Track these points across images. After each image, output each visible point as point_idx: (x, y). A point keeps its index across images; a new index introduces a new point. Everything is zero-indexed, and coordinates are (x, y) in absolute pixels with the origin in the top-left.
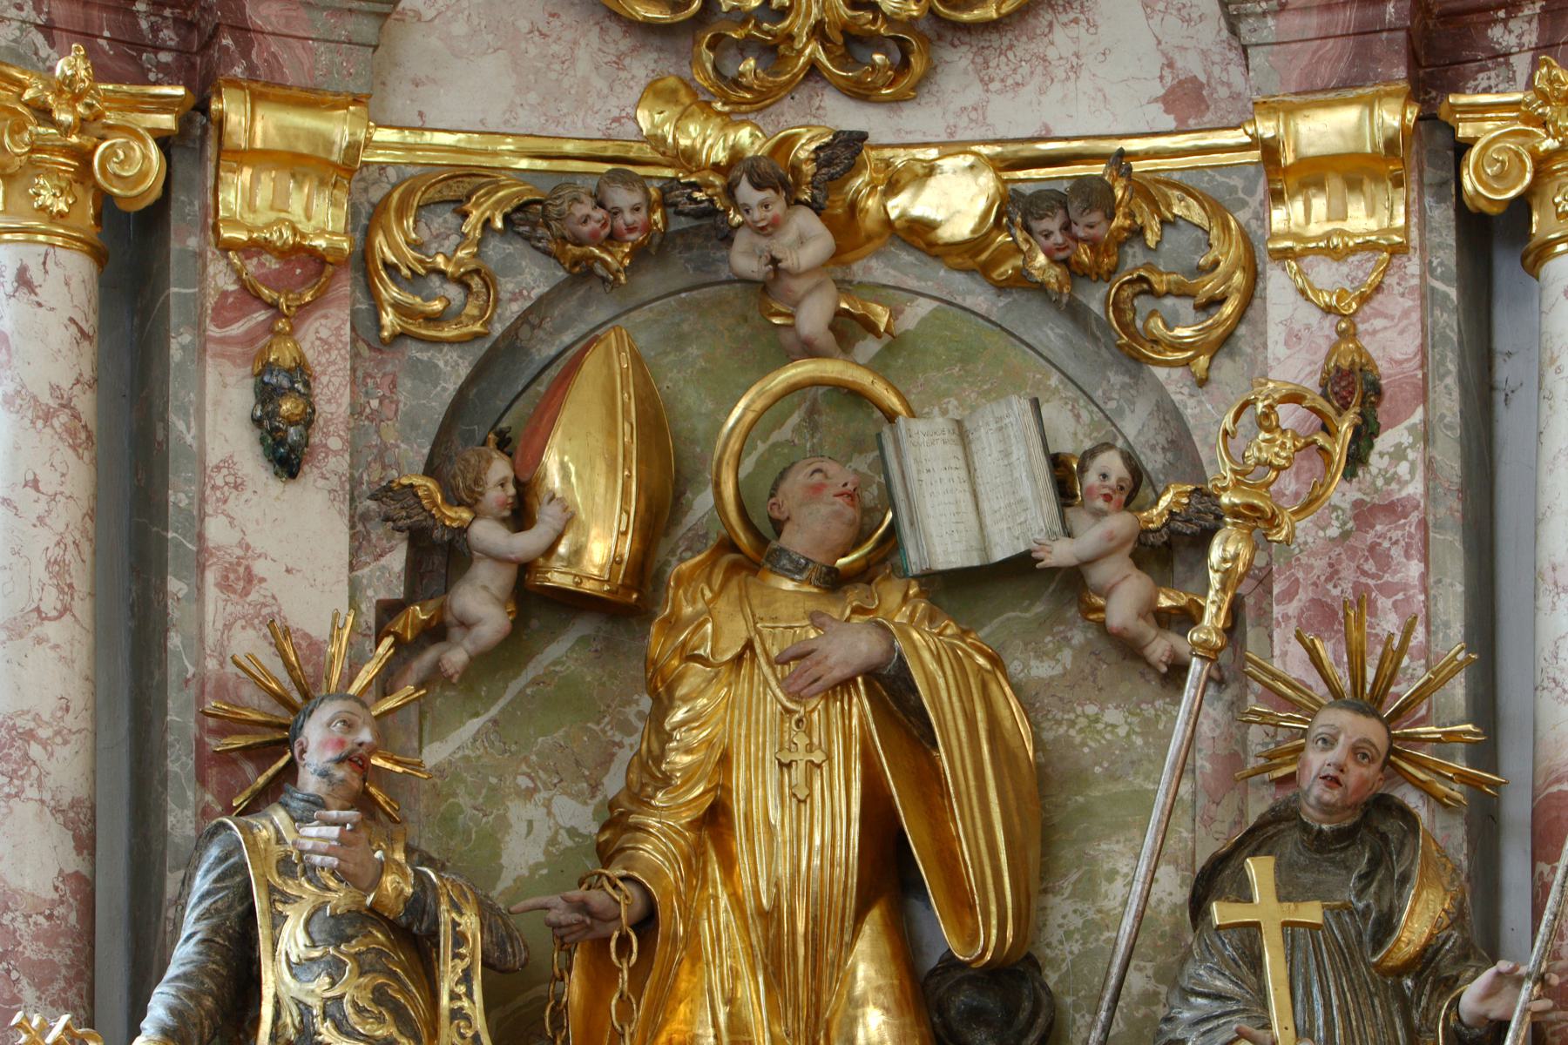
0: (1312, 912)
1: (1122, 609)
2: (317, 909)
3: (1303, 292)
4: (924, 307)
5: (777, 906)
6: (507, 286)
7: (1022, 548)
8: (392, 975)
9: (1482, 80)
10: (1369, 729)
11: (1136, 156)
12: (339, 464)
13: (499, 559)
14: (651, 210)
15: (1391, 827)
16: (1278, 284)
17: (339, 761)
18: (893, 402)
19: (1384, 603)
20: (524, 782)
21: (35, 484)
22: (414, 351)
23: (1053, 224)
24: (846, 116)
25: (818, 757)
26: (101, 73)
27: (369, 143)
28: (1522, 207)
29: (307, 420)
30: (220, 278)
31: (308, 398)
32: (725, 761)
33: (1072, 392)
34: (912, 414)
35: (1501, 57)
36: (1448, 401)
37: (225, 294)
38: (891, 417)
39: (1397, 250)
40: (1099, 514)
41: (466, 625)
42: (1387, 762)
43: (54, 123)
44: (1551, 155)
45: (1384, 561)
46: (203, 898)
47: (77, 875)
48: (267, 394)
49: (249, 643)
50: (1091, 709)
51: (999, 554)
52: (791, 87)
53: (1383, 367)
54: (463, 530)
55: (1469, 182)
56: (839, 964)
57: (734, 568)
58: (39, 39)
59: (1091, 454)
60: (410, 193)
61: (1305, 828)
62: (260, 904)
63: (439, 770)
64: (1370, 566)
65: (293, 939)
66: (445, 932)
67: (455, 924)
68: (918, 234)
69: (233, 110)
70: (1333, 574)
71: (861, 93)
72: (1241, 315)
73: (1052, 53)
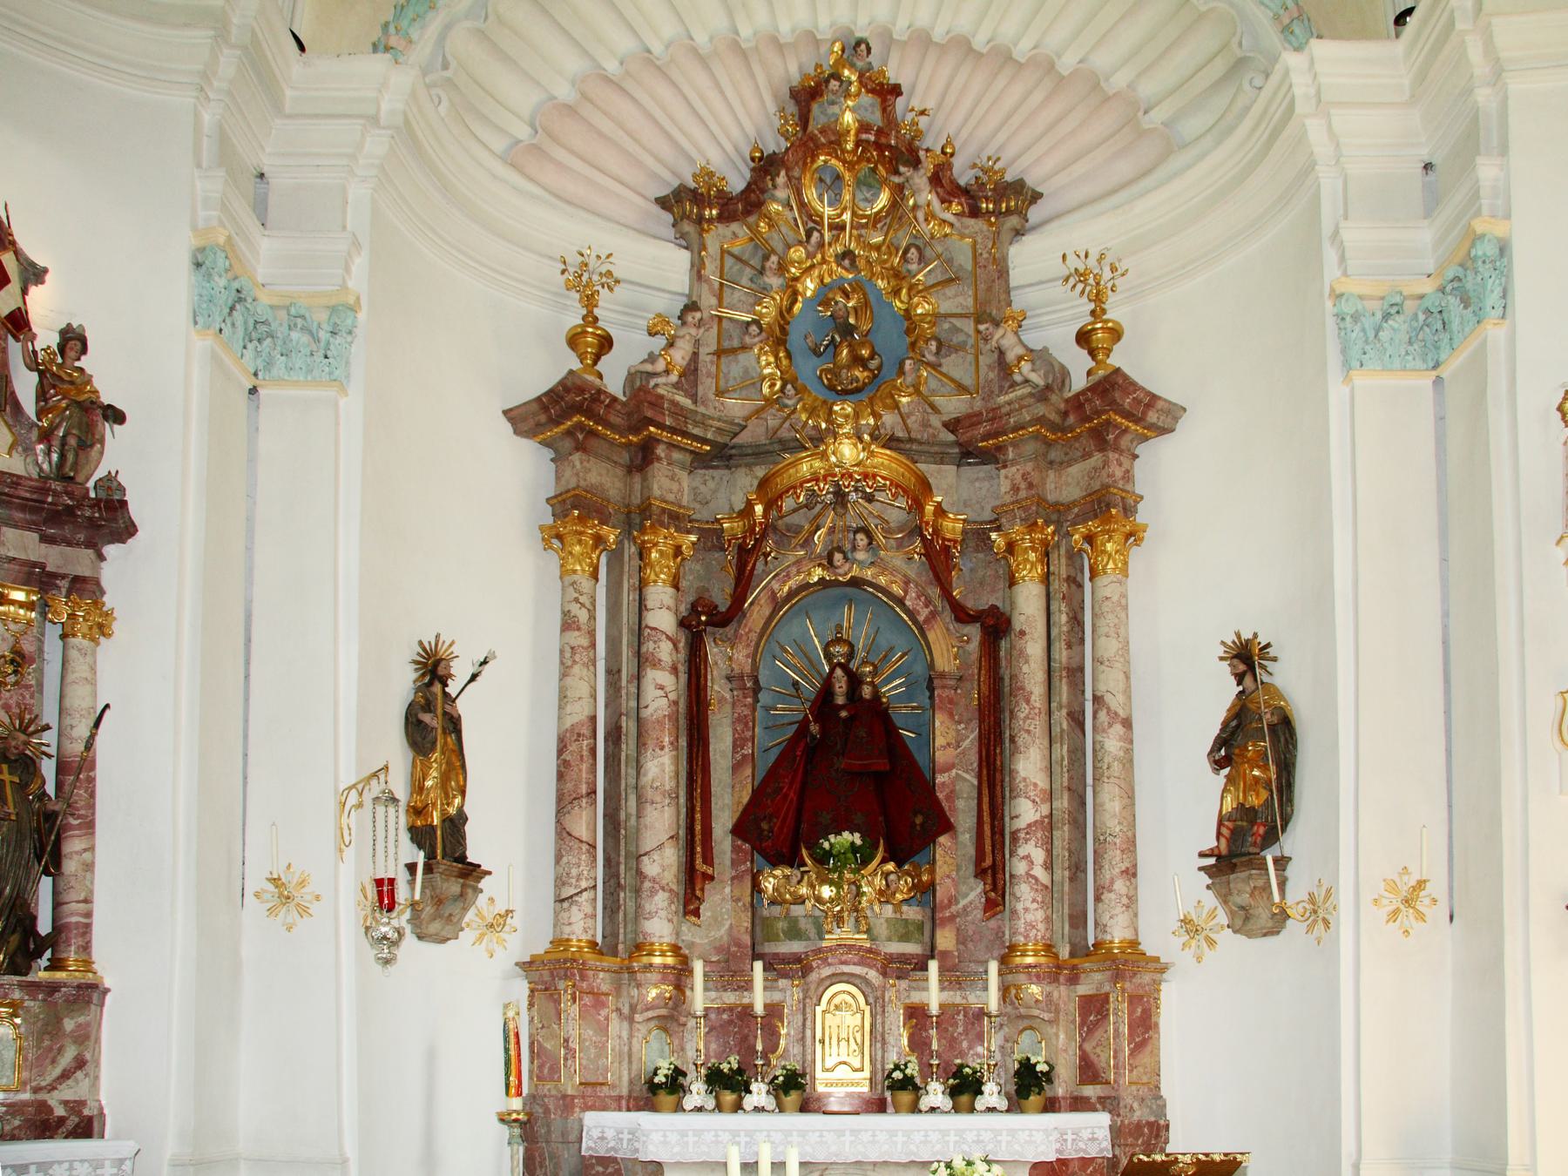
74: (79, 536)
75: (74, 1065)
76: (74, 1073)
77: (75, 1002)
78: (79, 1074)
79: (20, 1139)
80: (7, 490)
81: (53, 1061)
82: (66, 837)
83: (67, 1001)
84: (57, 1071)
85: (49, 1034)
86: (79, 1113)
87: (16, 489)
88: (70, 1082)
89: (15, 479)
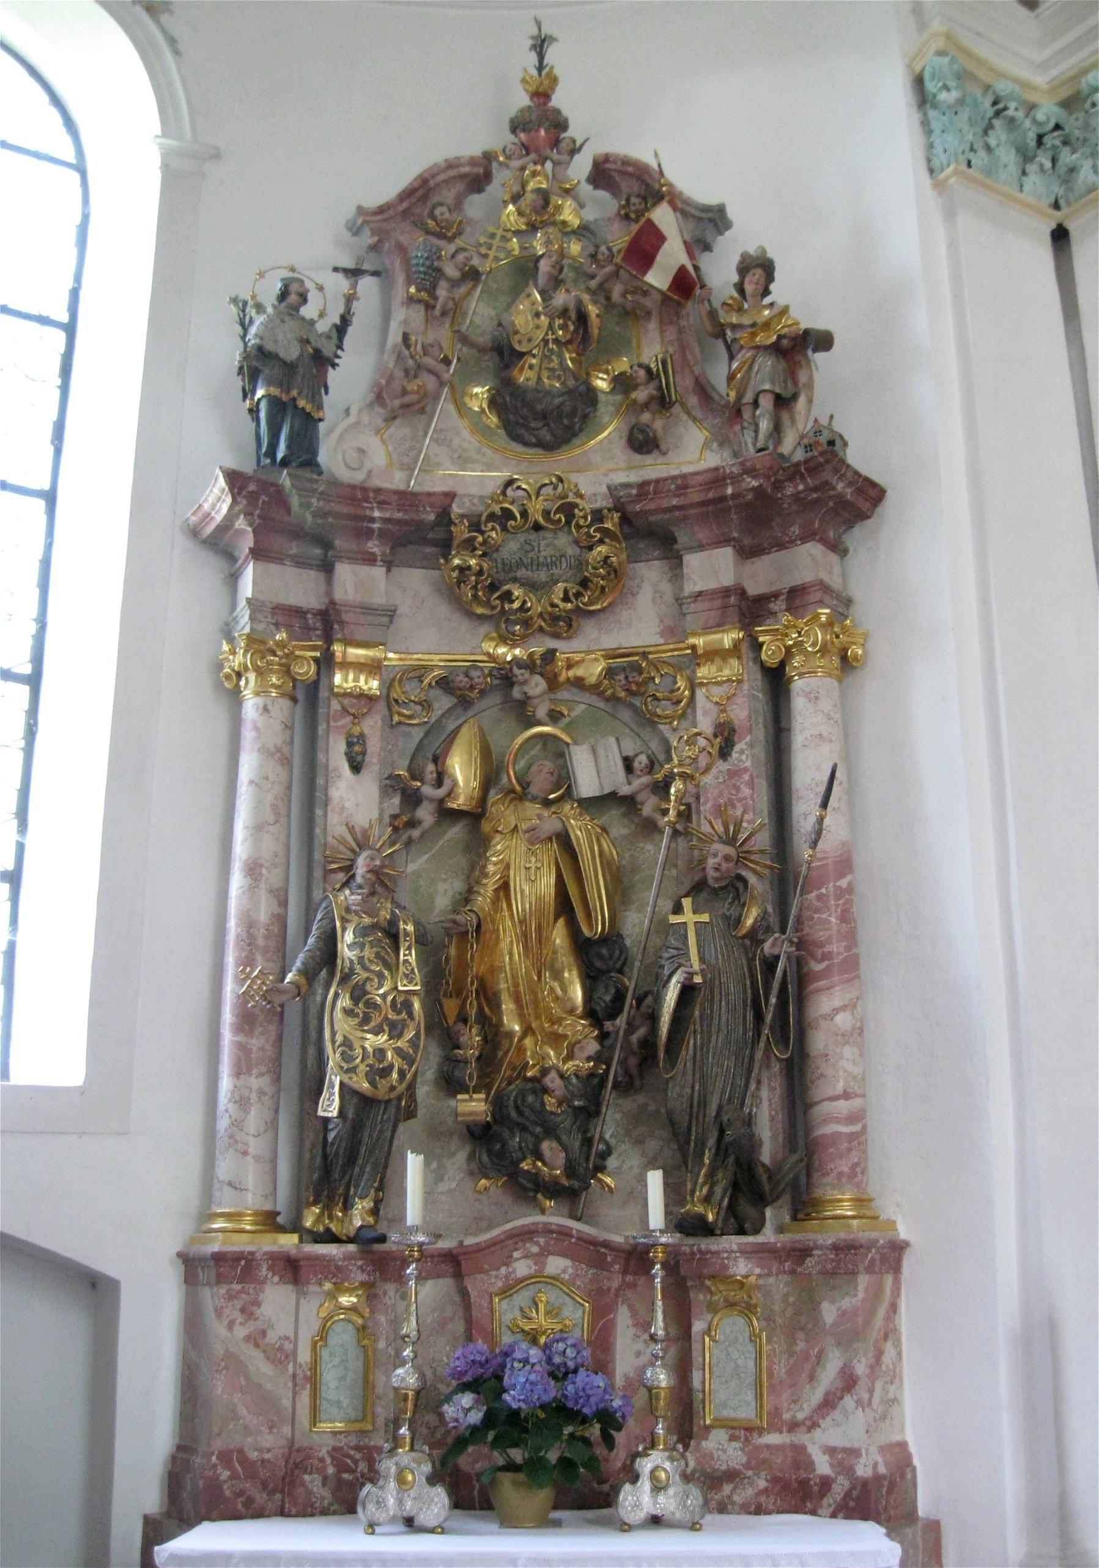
0: (705, 918)
1: (647, 810)
2: (358, 925)
3: (707, 697)
4: (583, 707)
5: (525, 920)
6: (436, 705)
7: (613, 789)
8: (383, 948)
9: (768, 622)
10: (730, 850)
11: (650, 653)
12: (376, 768)
13: (432, 800)
14: (485, 678)
15: (740, 885)
16: (700, 693)
17: (369, 872)
18: (568, 740)
19: (738, 805)
20: (443, 876)
21: (267, 778)
22: (404, 728)
23: (622, 677)
24: (552, 644)
25: (539, 865)
26: (292, 637)
27: (386, 659)
28: (782, 664)
29: (364, 753)
30: (335, 705)
31: (364, 744)
32: (508, 866)
33: (632, 734)
34: (576, 743)
35: (773, 614)
36: (760, 733)
37: (336, 711)
38: (568, 744)
39: (739, 682)
40: (639, 777)
41: (420, 822)
42: (738, 861)
43: (275, 655)
44: (791, 647)
45: (738, 789)
46: (321, 920)
47: (279, 915)
48: (350, 745)
49: (342, 831)
50: (641, 845)
51: (606, 791)
52: (532, 634)
53: (736, 722)
54: (418, 789)
55: (764, 657)
56: (548, 939)
57: (512, 800)
58: (273, 627)
59: (636, 755)
60: (403, 674)
61: (710, 887)
62: (338, 924)
63: (413, 873)
64: (733, 792)
65: (349, 937)
66: (401, 932)
67: (405, 929)
68: (578, 683)
69: (337, 648)
70: (721, 794)
71: (557, 636)
72: (688, 705)
73: (622, 619)
74: (792, 529)
75: (839, 1384)
76: (841, 1398)
77: (833, 1274)
78: (848, 1401)
79: (768, 1512)
80: (674, 502)
81: (812, 1378)
82: (818, 990)
83: (824, 1273)
84: (817, 1396)
85: (803, 1329)
86: (849, 1471)
87: (685, 494)
88: (836, 1414)
89: (679, 482)
